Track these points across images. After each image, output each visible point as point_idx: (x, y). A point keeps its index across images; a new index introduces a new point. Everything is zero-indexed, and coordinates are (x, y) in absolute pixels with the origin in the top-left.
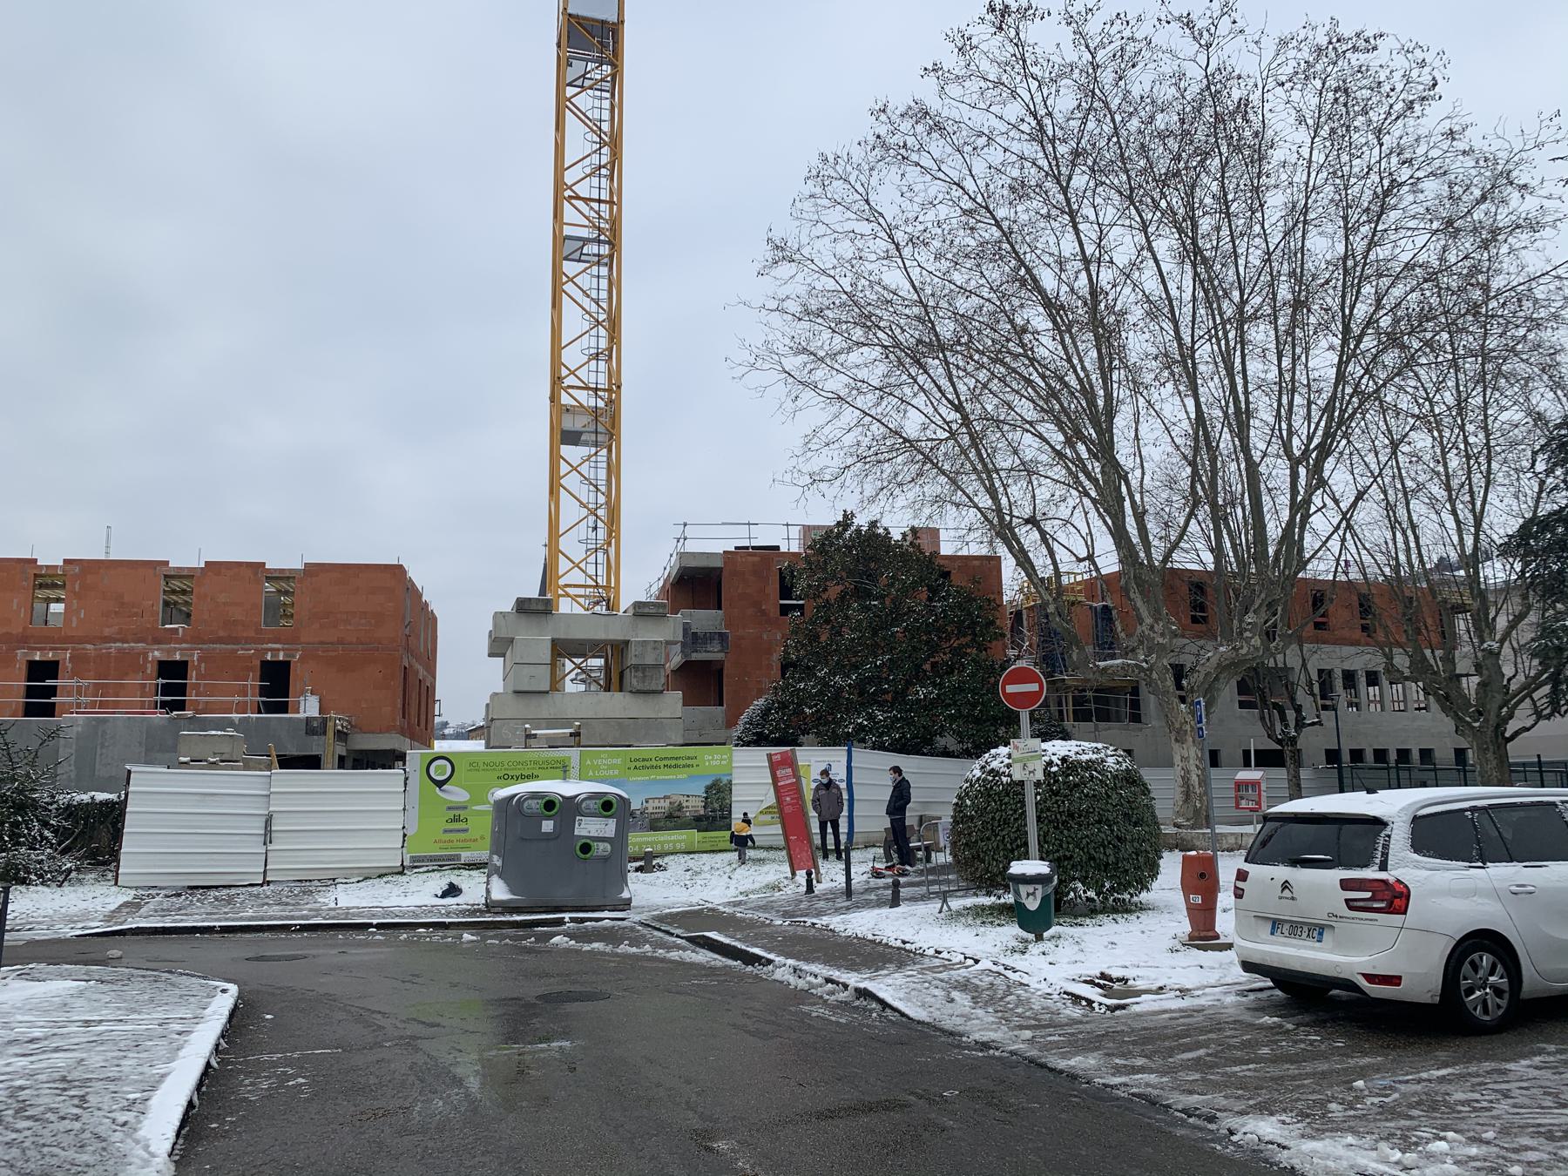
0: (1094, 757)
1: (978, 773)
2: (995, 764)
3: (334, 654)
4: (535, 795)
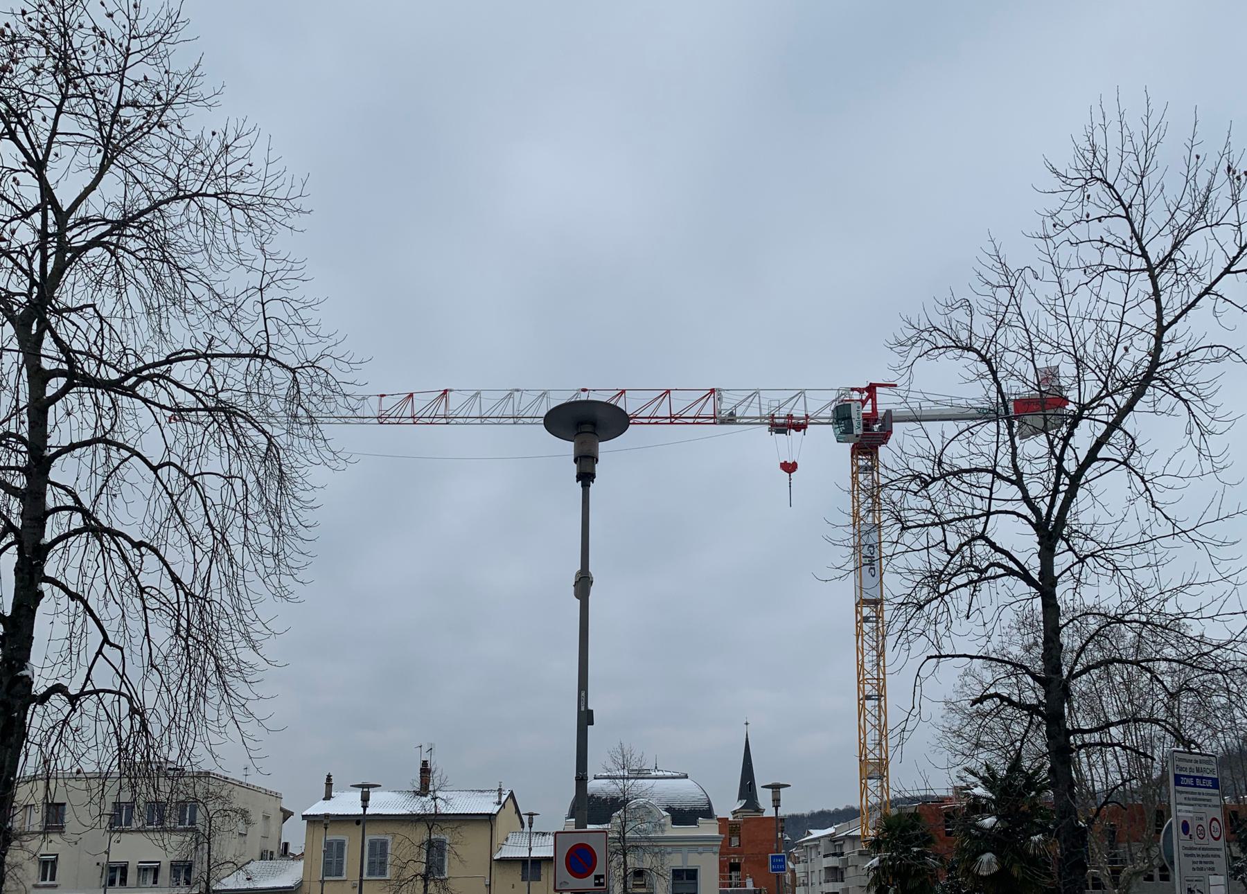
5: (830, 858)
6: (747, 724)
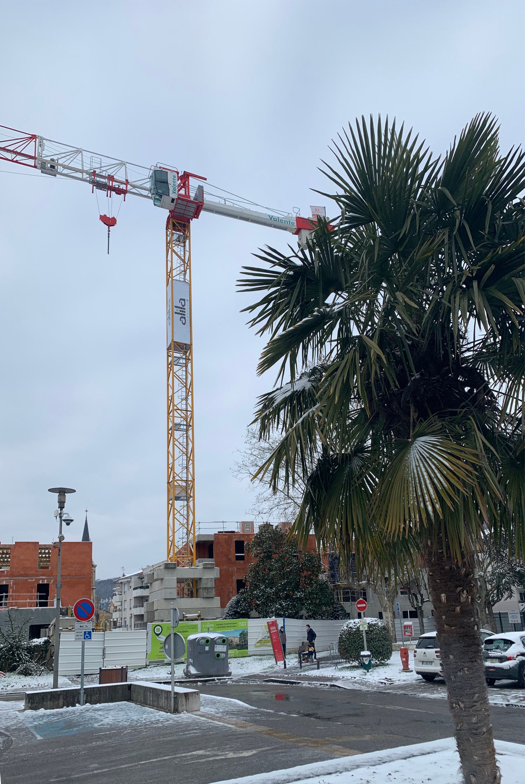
0: (376, 622)
1: (346, 628)
2: (351, 625)
3: (66, 580)
4: (203, 638)
5: (139, 590)
6: (87, 511)
